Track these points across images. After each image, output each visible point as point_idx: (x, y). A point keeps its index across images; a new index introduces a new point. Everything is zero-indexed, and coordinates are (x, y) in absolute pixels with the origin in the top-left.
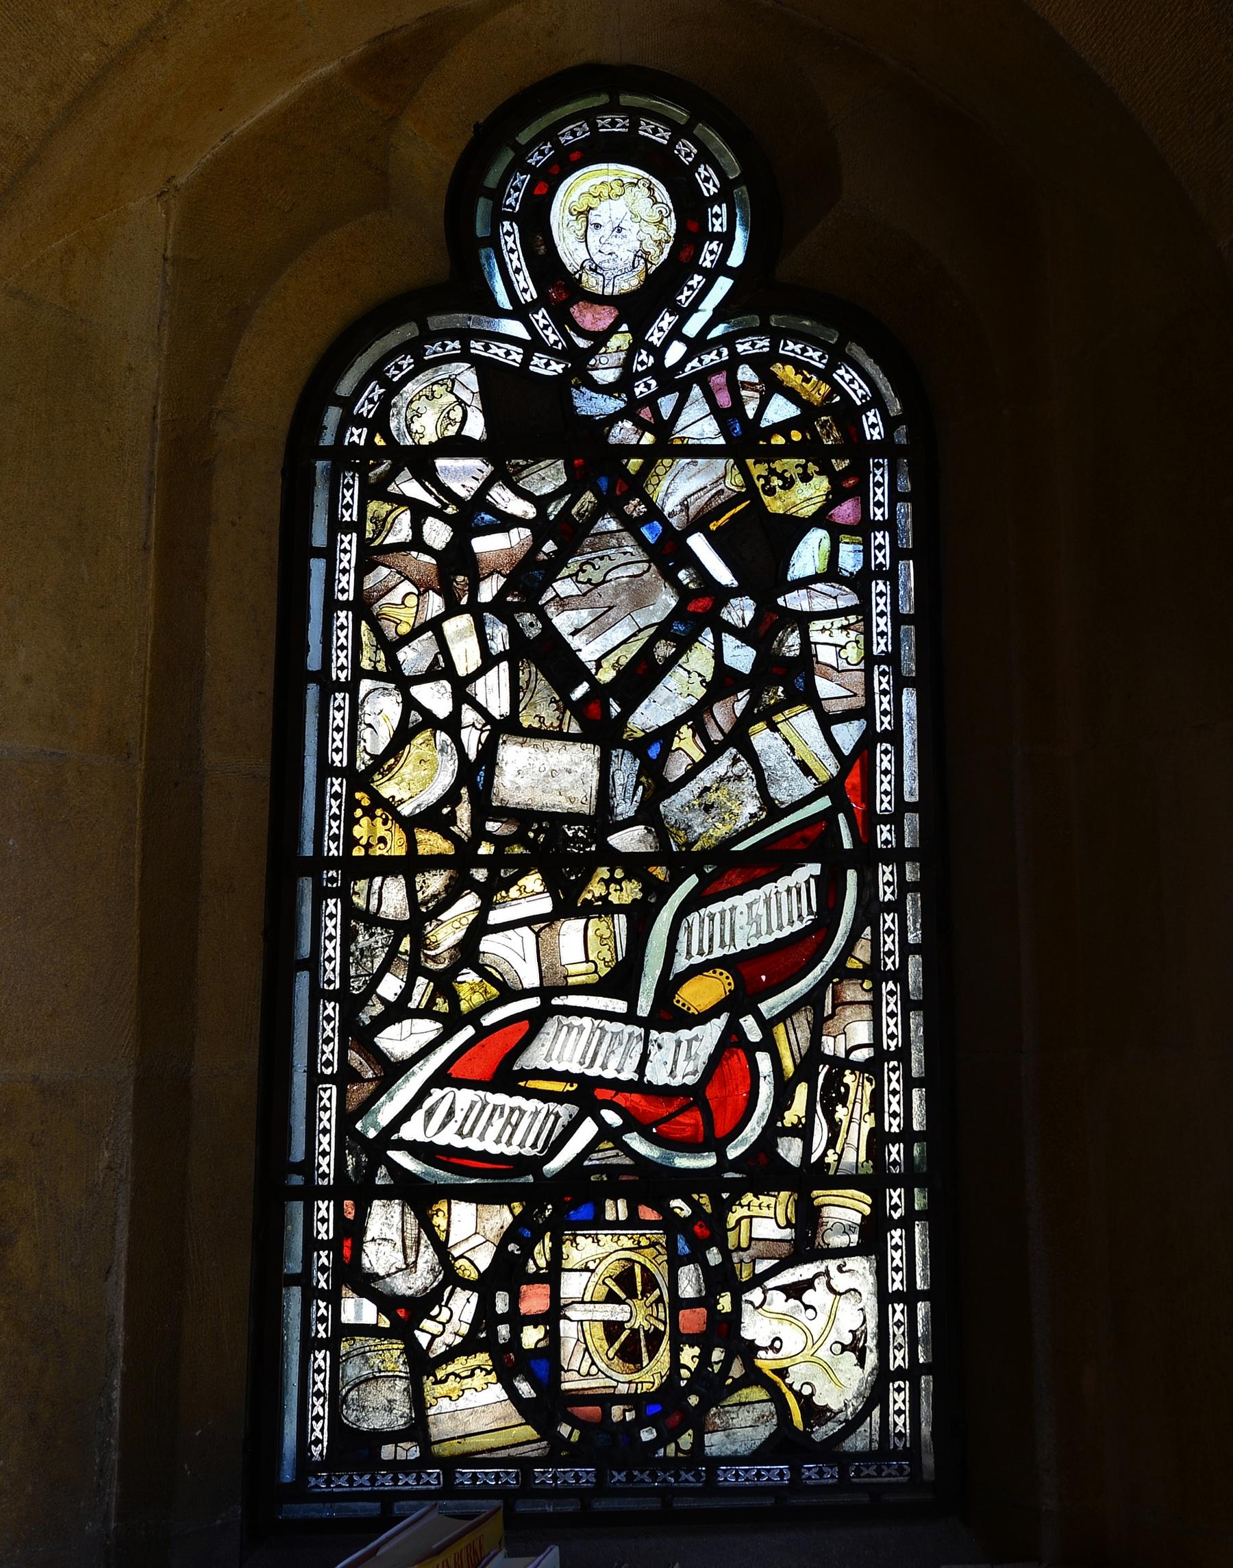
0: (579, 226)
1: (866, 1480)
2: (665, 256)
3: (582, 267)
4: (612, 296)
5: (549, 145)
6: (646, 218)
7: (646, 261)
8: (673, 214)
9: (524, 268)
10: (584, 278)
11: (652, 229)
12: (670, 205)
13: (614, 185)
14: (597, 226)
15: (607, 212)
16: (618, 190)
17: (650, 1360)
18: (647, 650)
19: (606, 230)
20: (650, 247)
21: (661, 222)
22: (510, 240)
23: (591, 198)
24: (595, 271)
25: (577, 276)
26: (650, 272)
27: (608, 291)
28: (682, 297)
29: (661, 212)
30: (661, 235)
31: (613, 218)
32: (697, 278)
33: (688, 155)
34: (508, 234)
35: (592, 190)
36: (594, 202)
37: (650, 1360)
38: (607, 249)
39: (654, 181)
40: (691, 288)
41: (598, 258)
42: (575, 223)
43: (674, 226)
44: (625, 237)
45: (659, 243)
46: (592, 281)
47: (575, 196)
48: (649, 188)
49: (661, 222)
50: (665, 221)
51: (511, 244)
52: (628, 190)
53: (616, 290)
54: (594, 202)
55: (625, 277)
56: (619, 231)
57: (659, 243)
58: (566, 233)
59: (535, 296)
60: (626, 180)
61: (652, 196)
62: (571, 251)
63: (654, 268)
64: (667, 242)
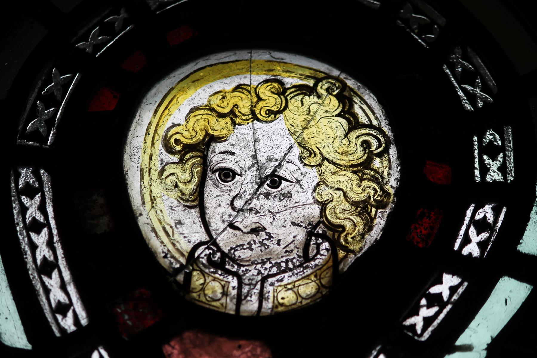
0: (185, 175)
1: (39, 287)
2: (375, 234)
3: (191, 258)
4: (257, 317)
5: (123, 15)
6: (333, 156)
7: (335, 245)
8: (393, 151)
9: (62, 263)
10: (197, 280)
11: (346, 180)
12: (387, 129)
13: (265, 92)
14: (227, 175)
15: (244, 146)
16: (271, 101)
17: (336, 116)
18: (305, 78)
19: (247, 182)
20: (341, 214)
21: (367, 164)
22: (33, 207)
23: (213, 119)
24: (219, 266)
25: (180, 278)
26: (344, 267)
27: (251, 306)
28: (417, 321)
29: (366, 145)
30: (369, 189)
31: (262, 158)
32: (449, 280)
33: (424, 29)
34: (30, 191)
35: (216, 101)
36: (220, 126)
37: (336, 116)
38: (248, 221)
39: (350, 83)
40: (436, 300)
41: (226, 240)
42: (177, 170)
43: (396, 174)
44: (288, 195)
45: (363, 208)
46: (214, 288)
47: (178, 114)
48: (340, 98)
49: (367, 164)
50: (377, 163)
51: (33, 212)
52: (294, 103)
53: (268, 305)
54: (220, 126)
55: (287, 278)
56: (275, 185)
57: (363, 208)
58: (157, 189)
59: (84, 321)
60: (290, 81)
61: (347, 113)
62: (166, 222)
63: (352, 258)
64: (380, 205)
